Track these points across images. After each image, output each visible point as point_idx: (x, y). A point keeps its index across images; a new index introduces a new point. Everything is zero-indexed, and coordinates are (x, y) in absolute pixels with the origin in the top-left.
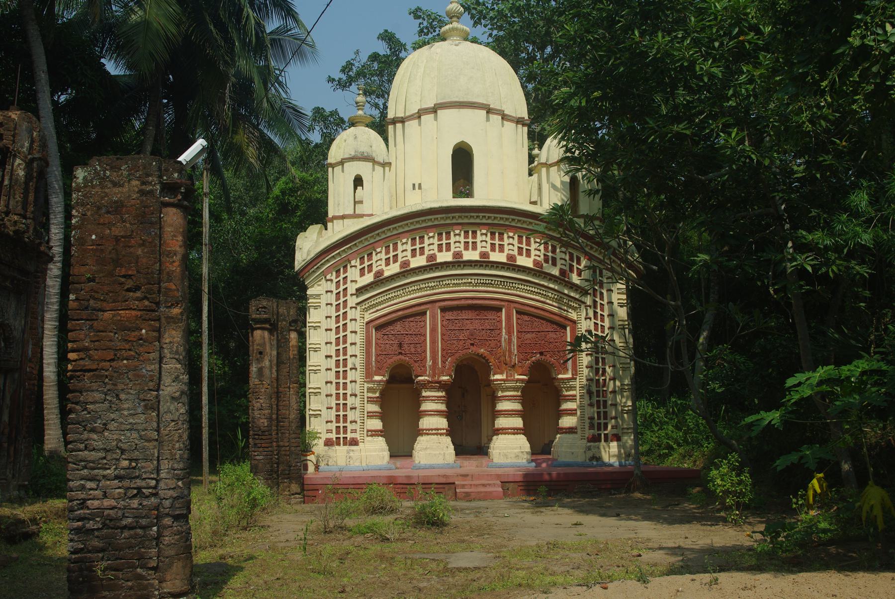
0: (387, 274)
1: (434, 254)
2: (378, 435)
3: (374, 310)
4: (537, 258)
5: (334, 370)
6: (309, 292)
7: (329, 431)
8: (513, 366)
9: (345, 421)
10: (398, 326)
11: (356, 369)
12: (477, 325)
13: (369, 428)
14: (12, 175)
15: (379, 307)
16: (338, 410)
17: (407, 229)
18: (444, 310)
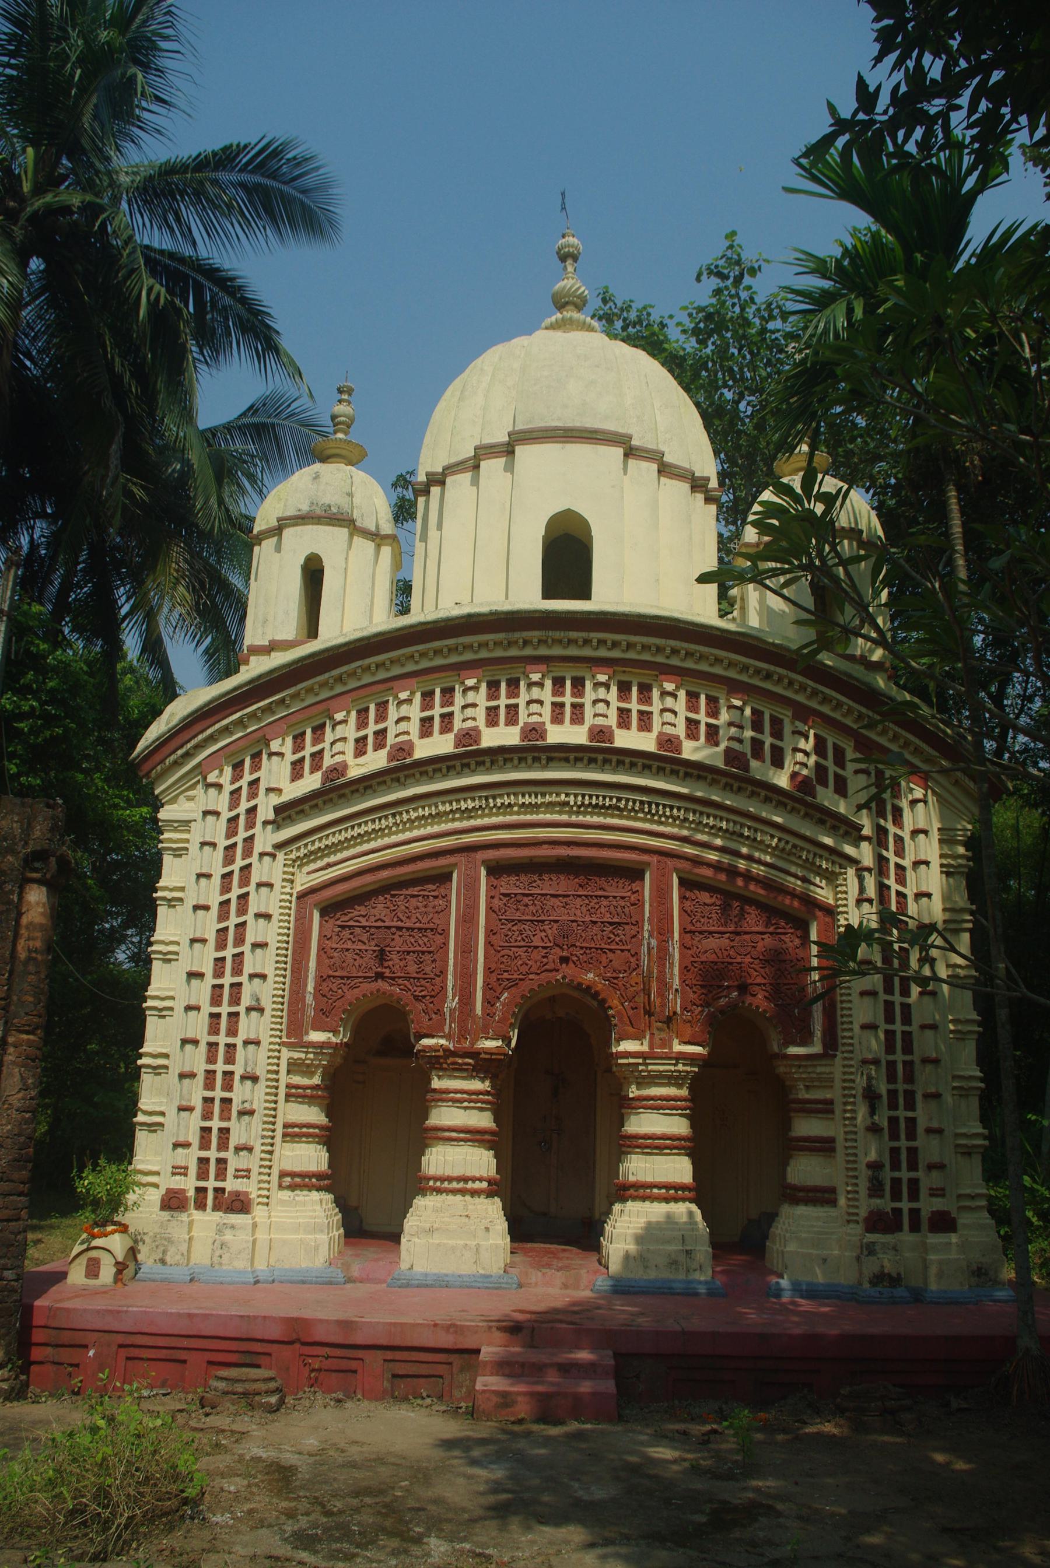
0: (354, 772)
1: (476, 729)
2: (310, 1188)
3: (320, 864)
4: (736, 745)
5: (207, 1009)
6: (163, 815)
7: (180, 1171)
8: (669, 1020)
9: (223, 1145)
10: (379, 908)
11: (261, 1010)
12: (578, 910)
13: (288, 1167)
15: (333, 859)
16: (207, 1116)
17: (410, 667)
18: (496, 870)
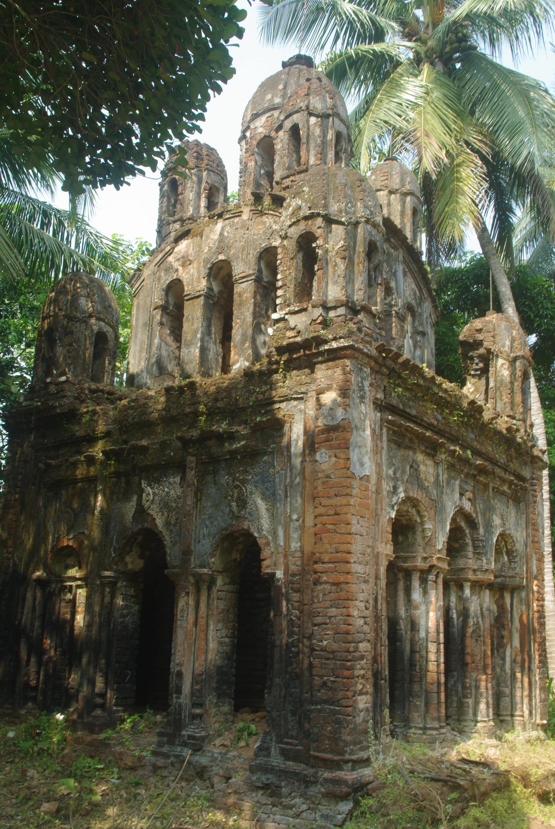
14: (496, 377)
